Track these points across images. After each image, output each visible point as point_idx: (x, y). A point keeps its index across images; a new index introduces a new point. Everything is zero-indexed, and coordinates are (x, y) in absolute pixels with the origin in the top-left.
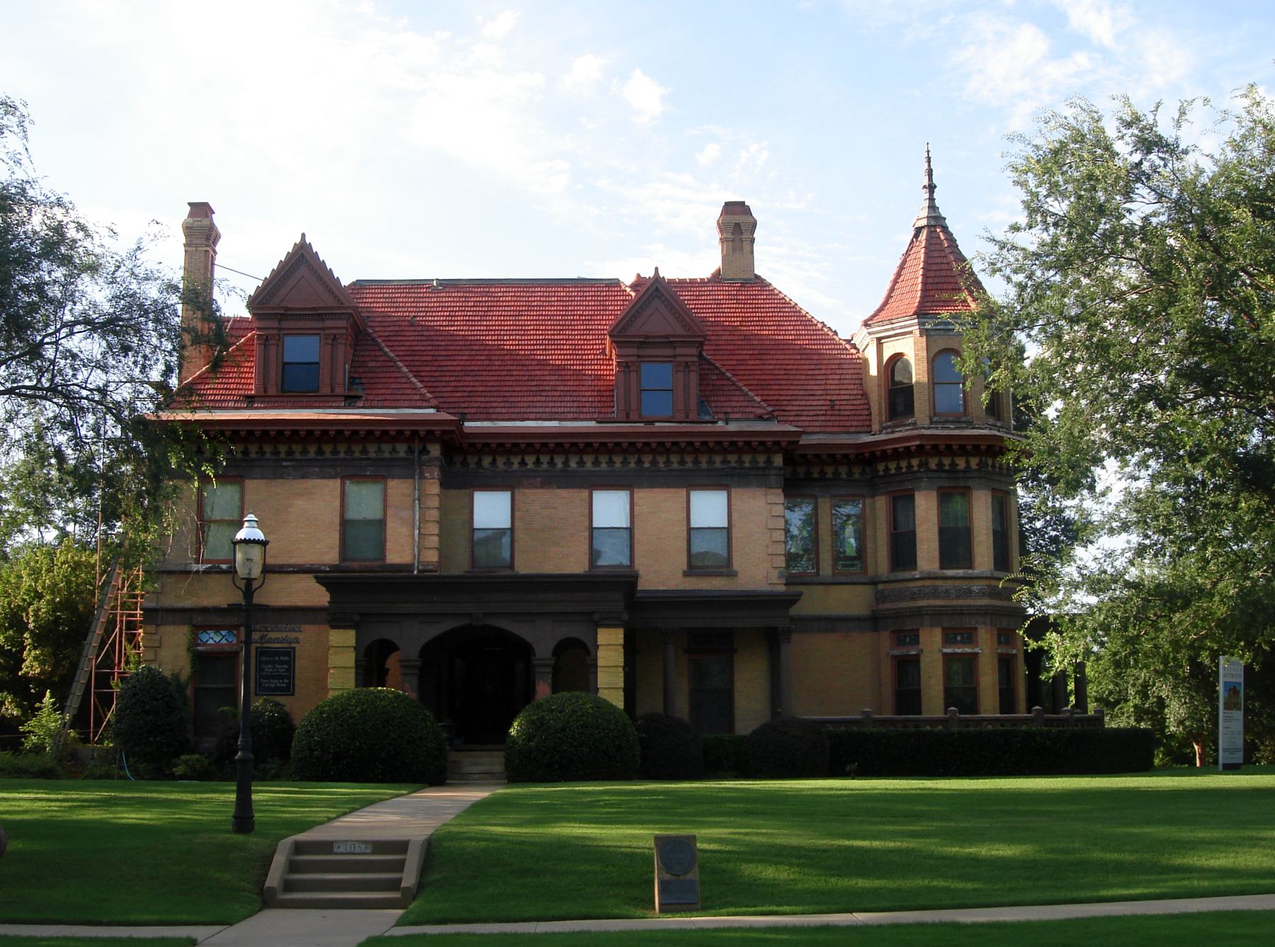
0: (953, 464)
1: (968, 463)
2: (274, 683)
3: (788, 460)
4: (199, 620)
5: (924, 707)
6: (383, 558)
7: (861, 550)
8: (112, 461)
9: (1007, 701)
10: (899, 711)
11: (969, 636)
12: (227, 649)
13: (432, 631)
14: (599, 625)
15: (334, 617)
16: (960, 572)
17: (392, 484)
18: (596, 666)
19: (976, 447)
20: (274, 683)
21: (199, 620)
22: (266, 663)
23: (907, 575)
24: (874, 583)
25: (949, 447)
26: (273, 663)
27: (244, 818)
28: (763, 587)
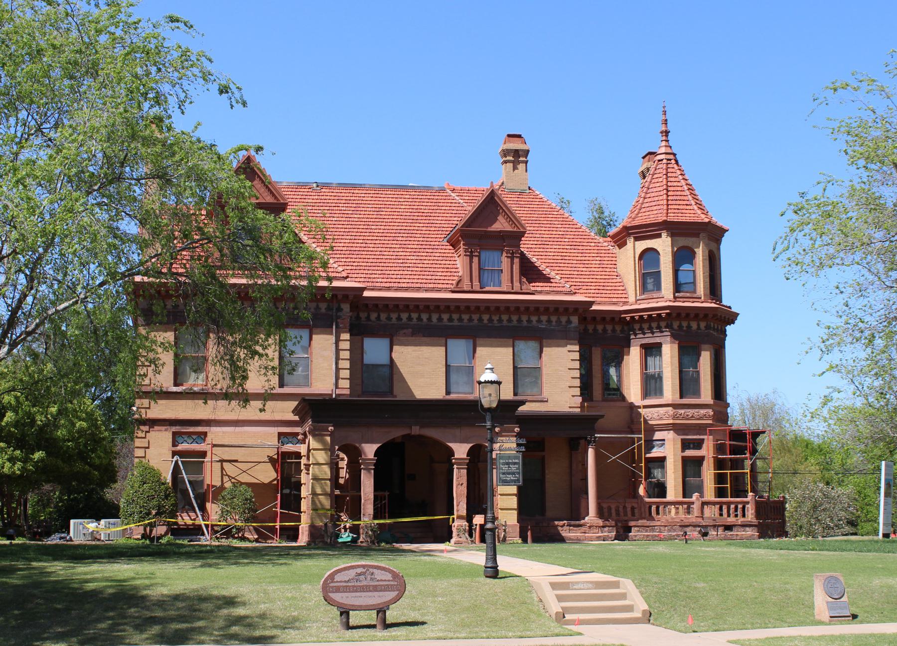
1: (698, 325)
3: (583, 320)
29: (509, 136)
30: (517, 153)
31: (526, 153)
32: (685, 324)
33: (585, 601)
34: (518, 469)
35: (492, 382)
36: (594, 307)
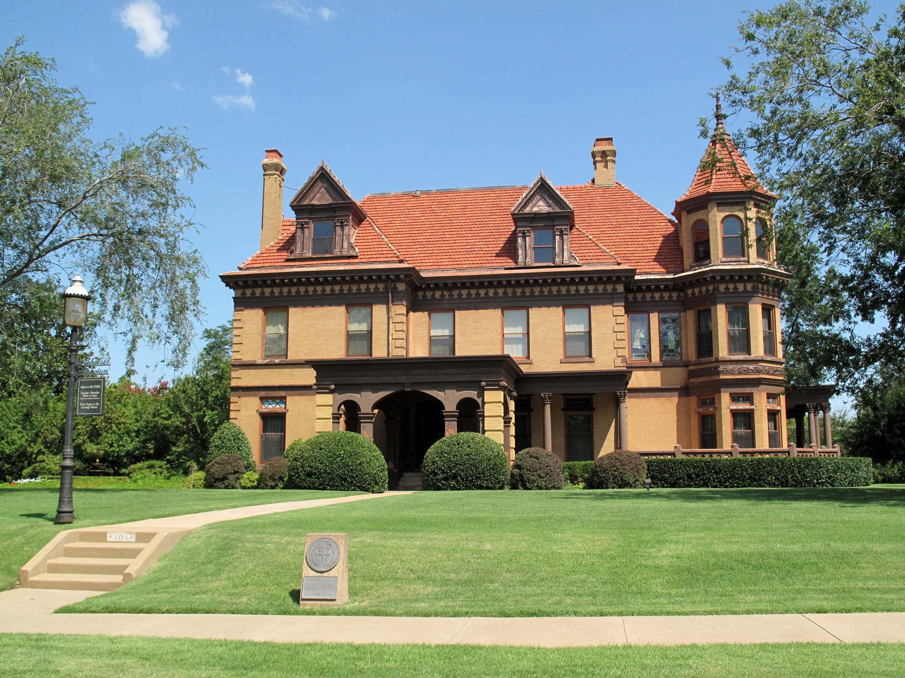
0: (735, 288)
1: (745, 287)
3: (628, 290)
5: (757, 444)
7: (678, 343)
9: (774, 439)
10: (703, 446)
15: (321, 387)
16: (741, 357)
17: (536, 314)
18: (483, 416)
19: (609, 278)
21: (263, 393)
22: (84, 390)
23: (706, 359)
24: (686, 365)
25: (591, 279)
26: (89, 390)
28: (611, 368)
29: (597, 140)
30: (604, 154)
31: (614, 153)
32: (731, 286)
33: (891, 490)
34: (99, 396)
35: (81, 297)
36: (637, 277)
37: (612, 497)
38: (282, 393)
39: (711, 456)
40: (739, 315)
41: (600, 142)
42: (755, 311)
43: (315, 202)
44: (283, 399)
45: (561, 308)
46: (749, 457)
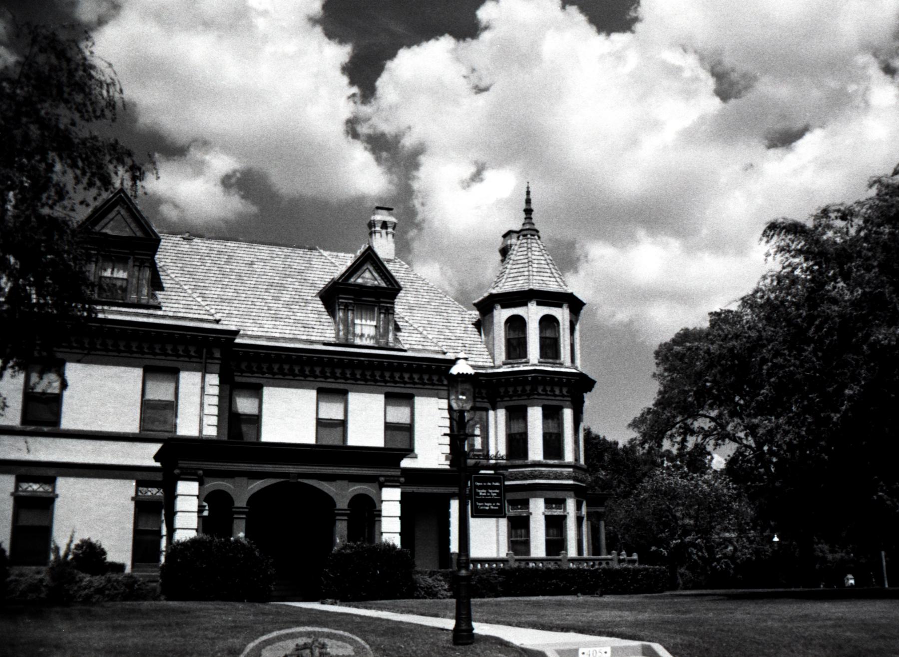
2: (488, 506)
4: (23, 470)
6: (175, 432)
8: (760, 338)
9: (555, 544)
11: (561, 503)
12: (44, 495)
13: (257, 485)
14: (382, 485)
16: (556, 462)
20: (488, 506)
21: (140, 475)
22: (481, 488)
26: (486, 488)
27: (463, 635)
34: (498, 494)
37: (579, 605)
38: (51, 472)
39: (607, 564)
40: (517, 415)
41: (380, 211)
42: (535, 415)
43: (107, 231)
44: (52, 481)
45: (138, 372)
46: (523, 565)
